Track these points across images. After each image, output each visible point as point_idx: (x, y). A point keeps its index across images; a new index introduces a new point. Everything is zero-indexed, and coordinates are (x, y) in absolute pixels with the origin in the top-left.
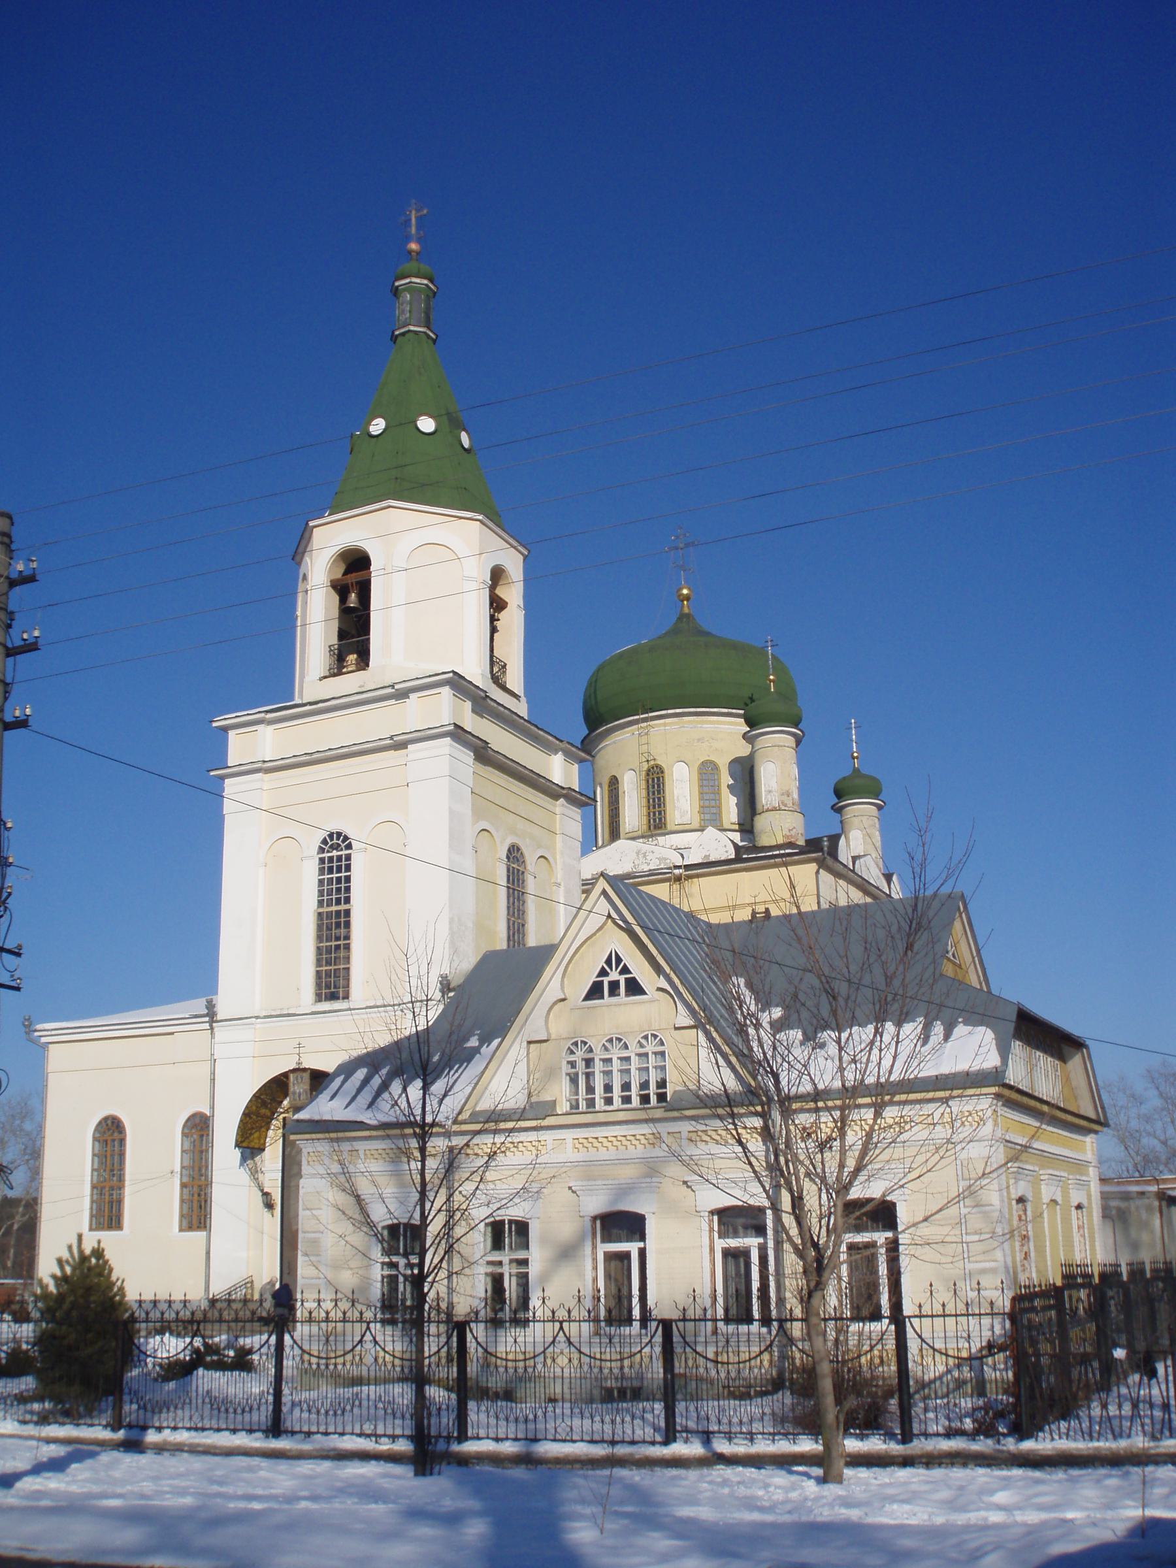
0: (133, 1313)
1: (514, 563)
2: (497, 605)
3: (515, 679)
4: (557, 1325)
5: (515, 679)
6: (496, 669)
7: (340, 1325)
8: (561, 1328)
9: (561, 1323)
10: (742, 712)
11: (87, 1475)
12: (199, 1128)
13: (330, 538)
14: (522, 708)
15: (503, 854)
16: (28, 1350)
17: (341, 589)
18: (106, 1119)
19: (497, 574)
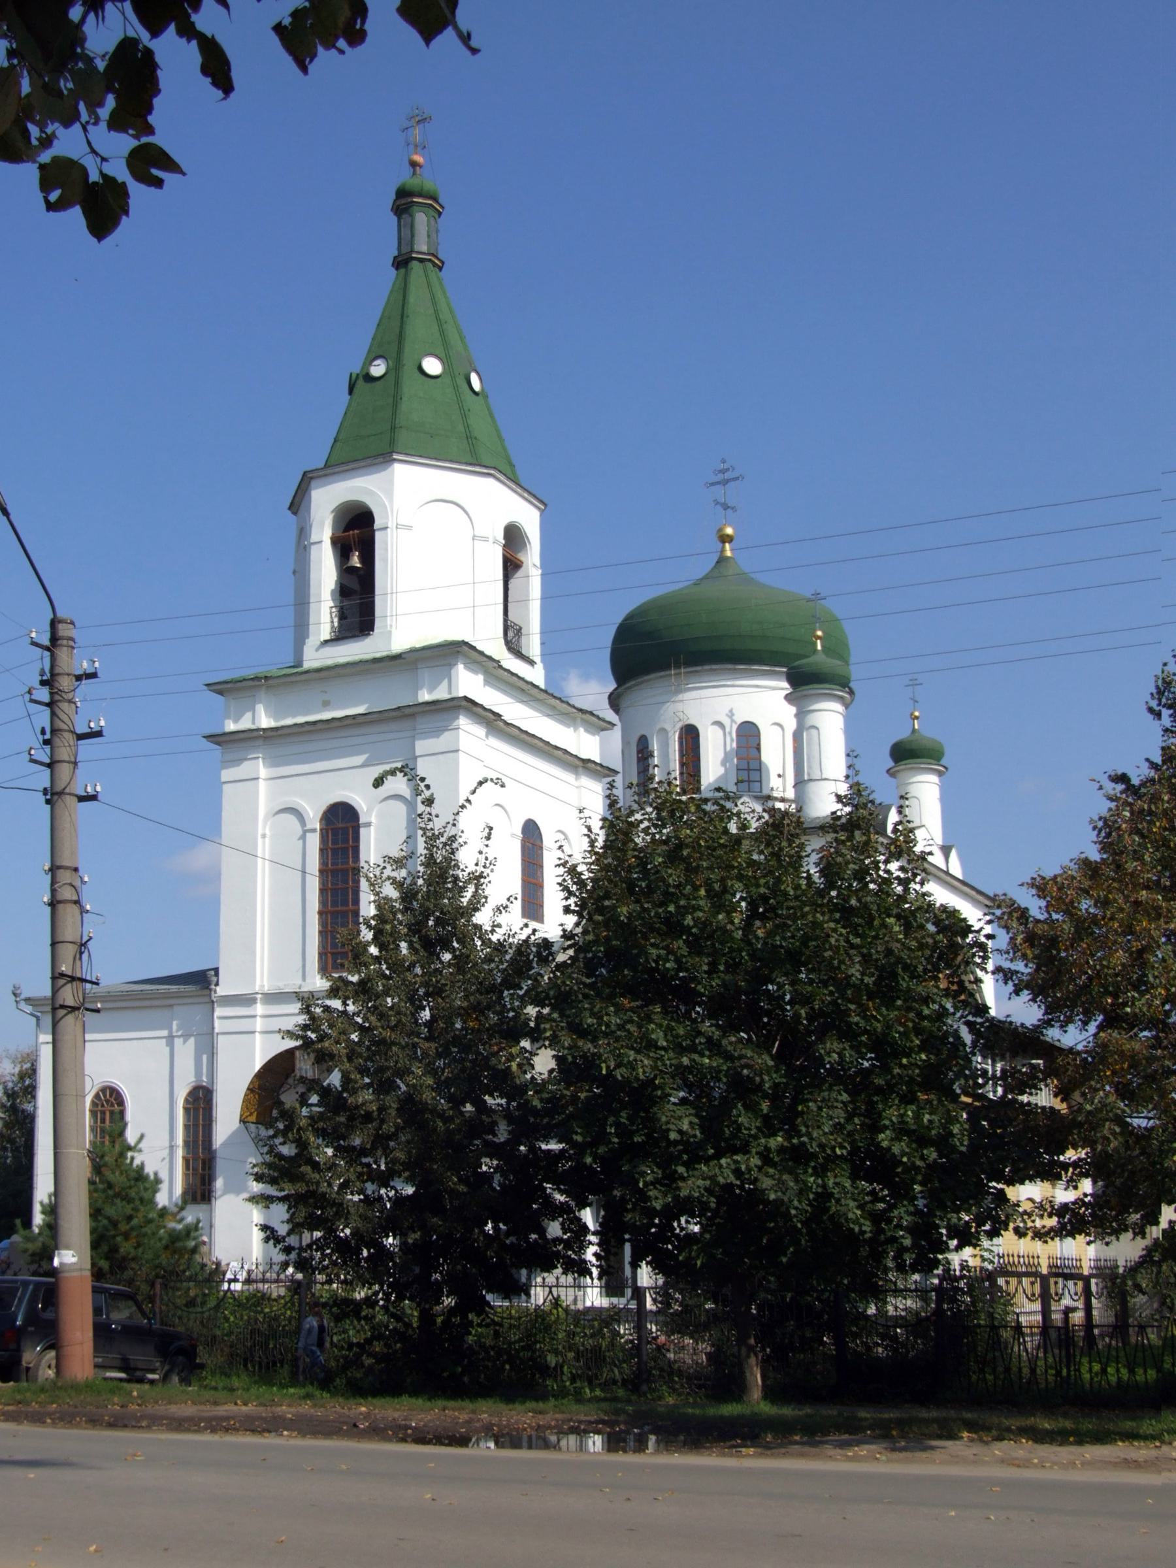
0: (684, 1179)
1: (529, 519)
2: (511, 566)
3: (533, 645)
4: (547, 1289)
5: (533, 645)
6: (511, 634)
7: (571, 1291)
8: (551, 1292)
9: (550, 1288)
10: (785, 670)
11: (78, 1334)
12: (200, 1103)
13: (326, 501)
14: (536, 675)
15: (518, 830)
16: (327, 1146)
17: (342, 548)
18: (103, 1090)
19: (513, 537)
